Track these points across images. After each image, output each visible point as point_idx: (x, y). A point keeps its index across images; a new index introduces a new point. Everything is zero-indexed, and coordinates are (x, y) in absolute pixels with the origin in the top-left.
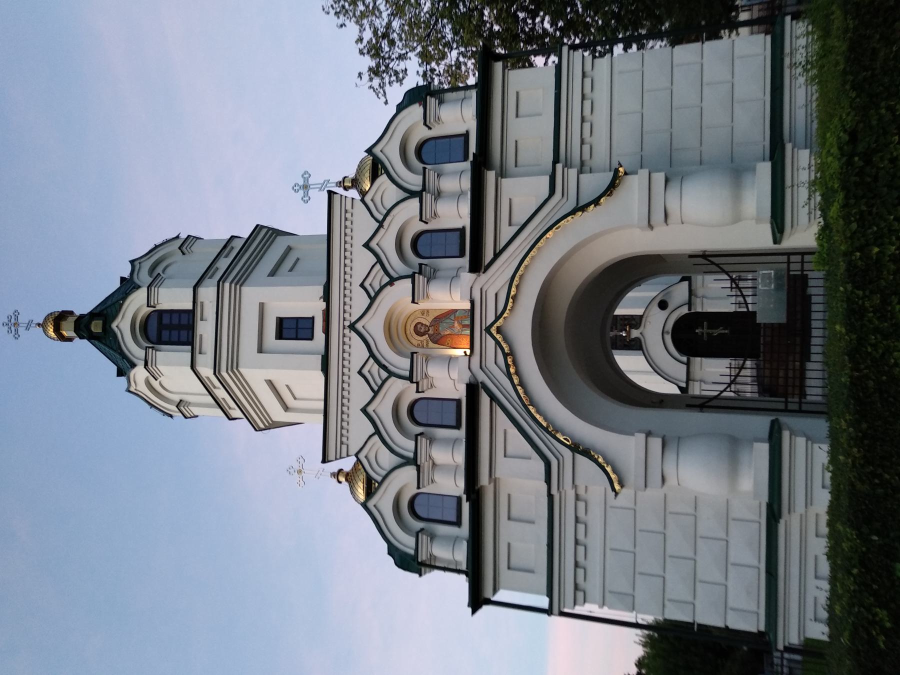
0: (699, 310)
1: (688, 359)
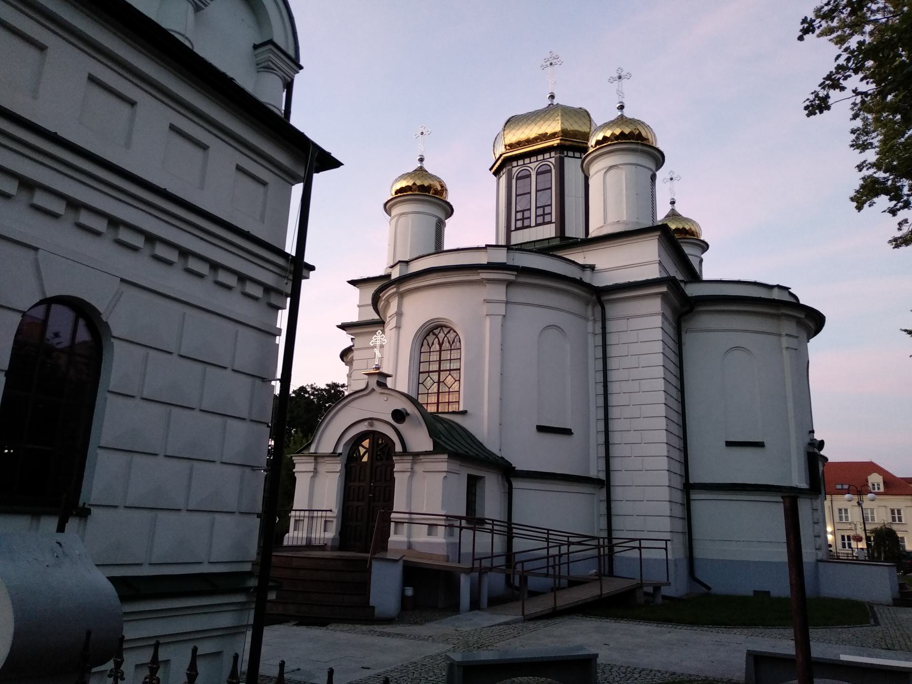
0: (397, 467)
1: (340, 454)
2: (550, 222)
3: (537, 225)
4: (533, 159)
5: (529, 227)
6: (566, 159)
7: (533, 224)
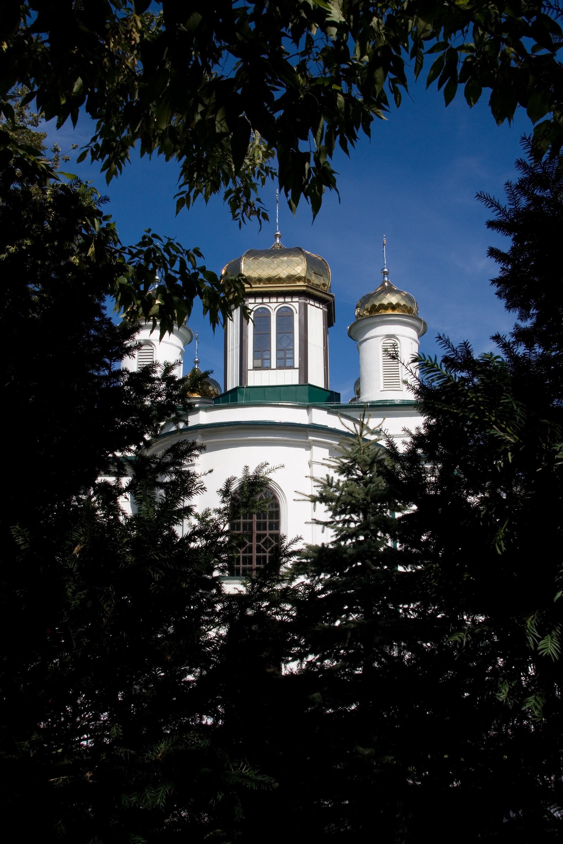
2: (292, 367)
3: (279, 368)
4: (274, 300)
5: (269, 368)
6: (309, 306)
7: (274, 365)
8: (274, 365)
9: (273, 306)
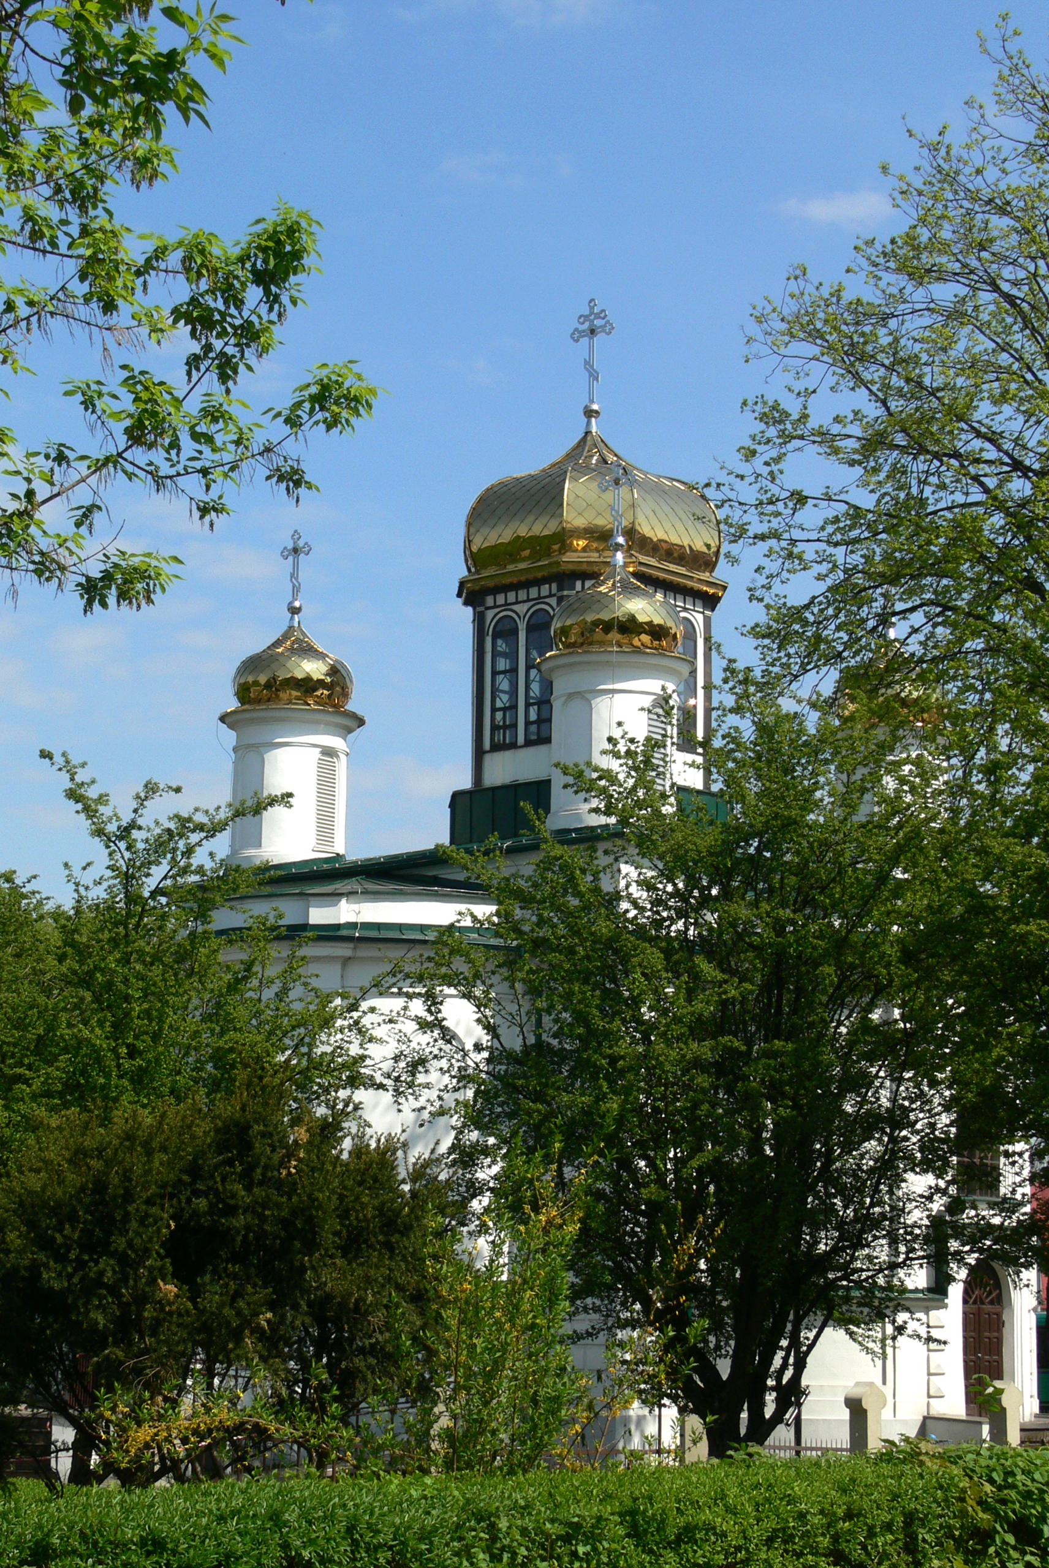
4: (522, 595)
5: (513, 746)
7: (521, 740)
8: (521, 740)
9: (521, 609)
